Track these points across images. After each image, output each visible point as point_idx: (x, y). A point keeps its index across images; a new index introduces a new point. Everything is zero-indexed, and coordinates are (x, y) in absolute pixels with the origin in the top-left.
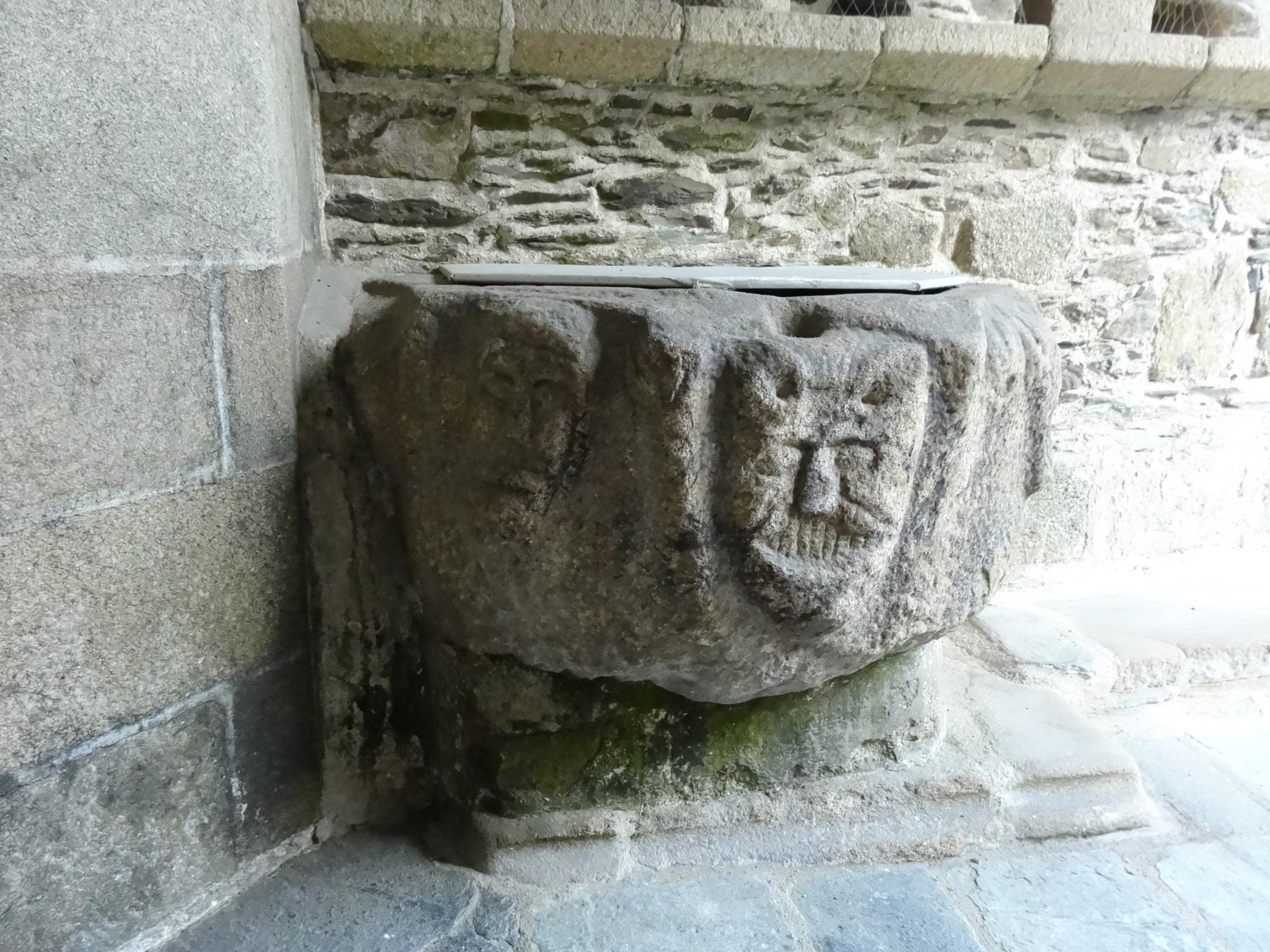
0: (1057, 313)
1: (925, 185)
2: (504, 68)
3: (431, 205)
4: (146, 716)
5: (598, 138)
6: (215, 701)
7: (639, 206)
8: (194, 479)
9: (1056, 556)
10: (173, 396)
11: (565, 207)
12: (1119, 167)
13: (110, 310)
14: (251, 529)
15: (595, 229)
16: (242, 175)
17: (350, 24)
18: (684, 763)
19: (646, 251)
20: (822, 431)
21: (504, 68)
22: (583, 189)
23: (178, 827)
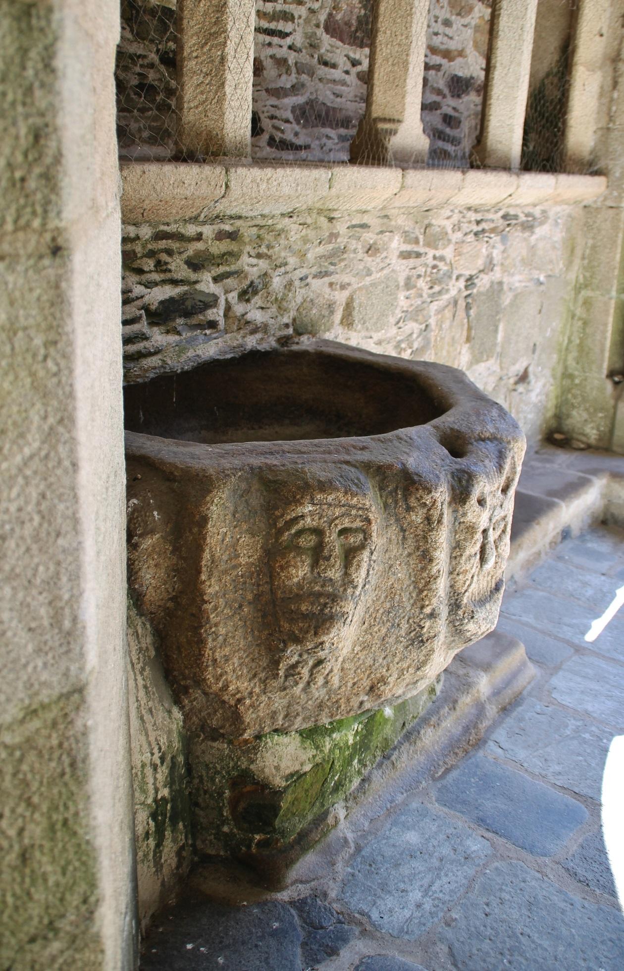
5: (146, 269)
7: (174, 320)
15: (147, 346)
19: (179, 356)
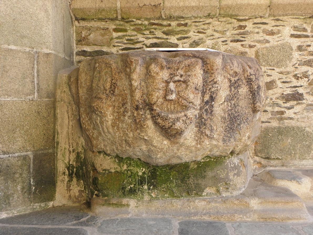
0: (291, 77)
2: (119, 17)
4: (11, 153)
5: (145, 33)
8: (28, 98)
9: (304, 157)
10: (24, 78)
12: (305, 33)
13: (12, 57)
14: (41, 114)
16: (44, 32)
17: (81, 8)
18: (151, 186)
20: (171, 78)
21: (119, 17)
22: (142, 46)
23: (16, 186)
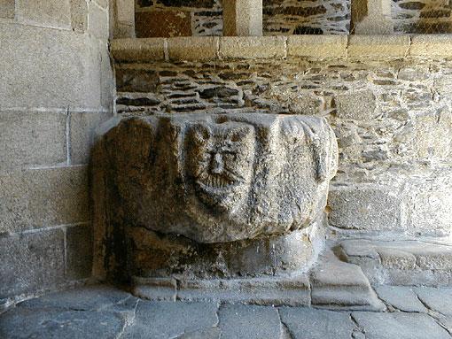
1: (315, 87)
2: (167, 58)
3: (146, 99)
6: (60, 229)
11: (188, 98)
21: (167, 58)
